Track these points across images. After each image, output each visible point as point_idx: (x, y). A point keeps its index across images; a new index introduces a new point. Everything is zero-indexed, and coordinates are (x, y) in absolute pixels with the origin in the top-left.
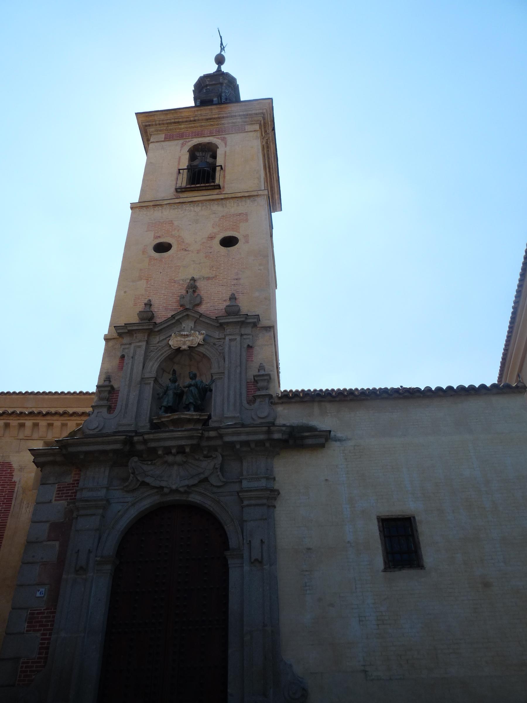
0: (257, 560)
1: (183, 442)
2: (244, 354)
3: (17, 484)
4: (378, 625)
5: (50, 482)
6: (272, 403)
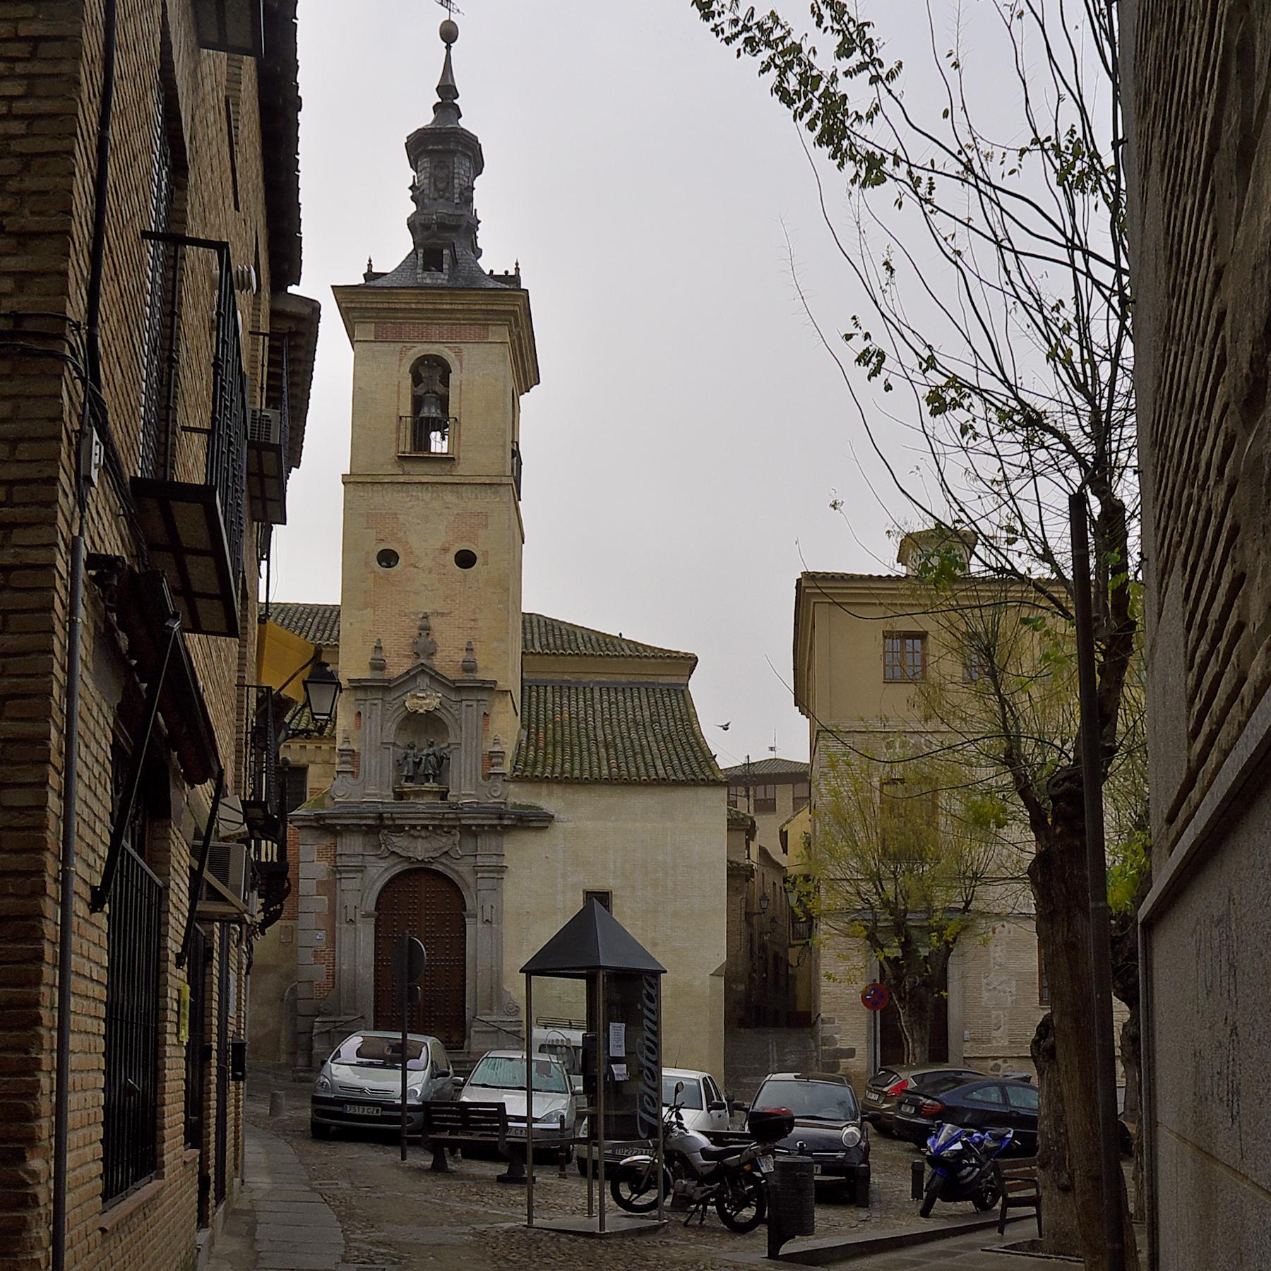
1: (426, 822)
2: (481, 723)
5: (208, 805)
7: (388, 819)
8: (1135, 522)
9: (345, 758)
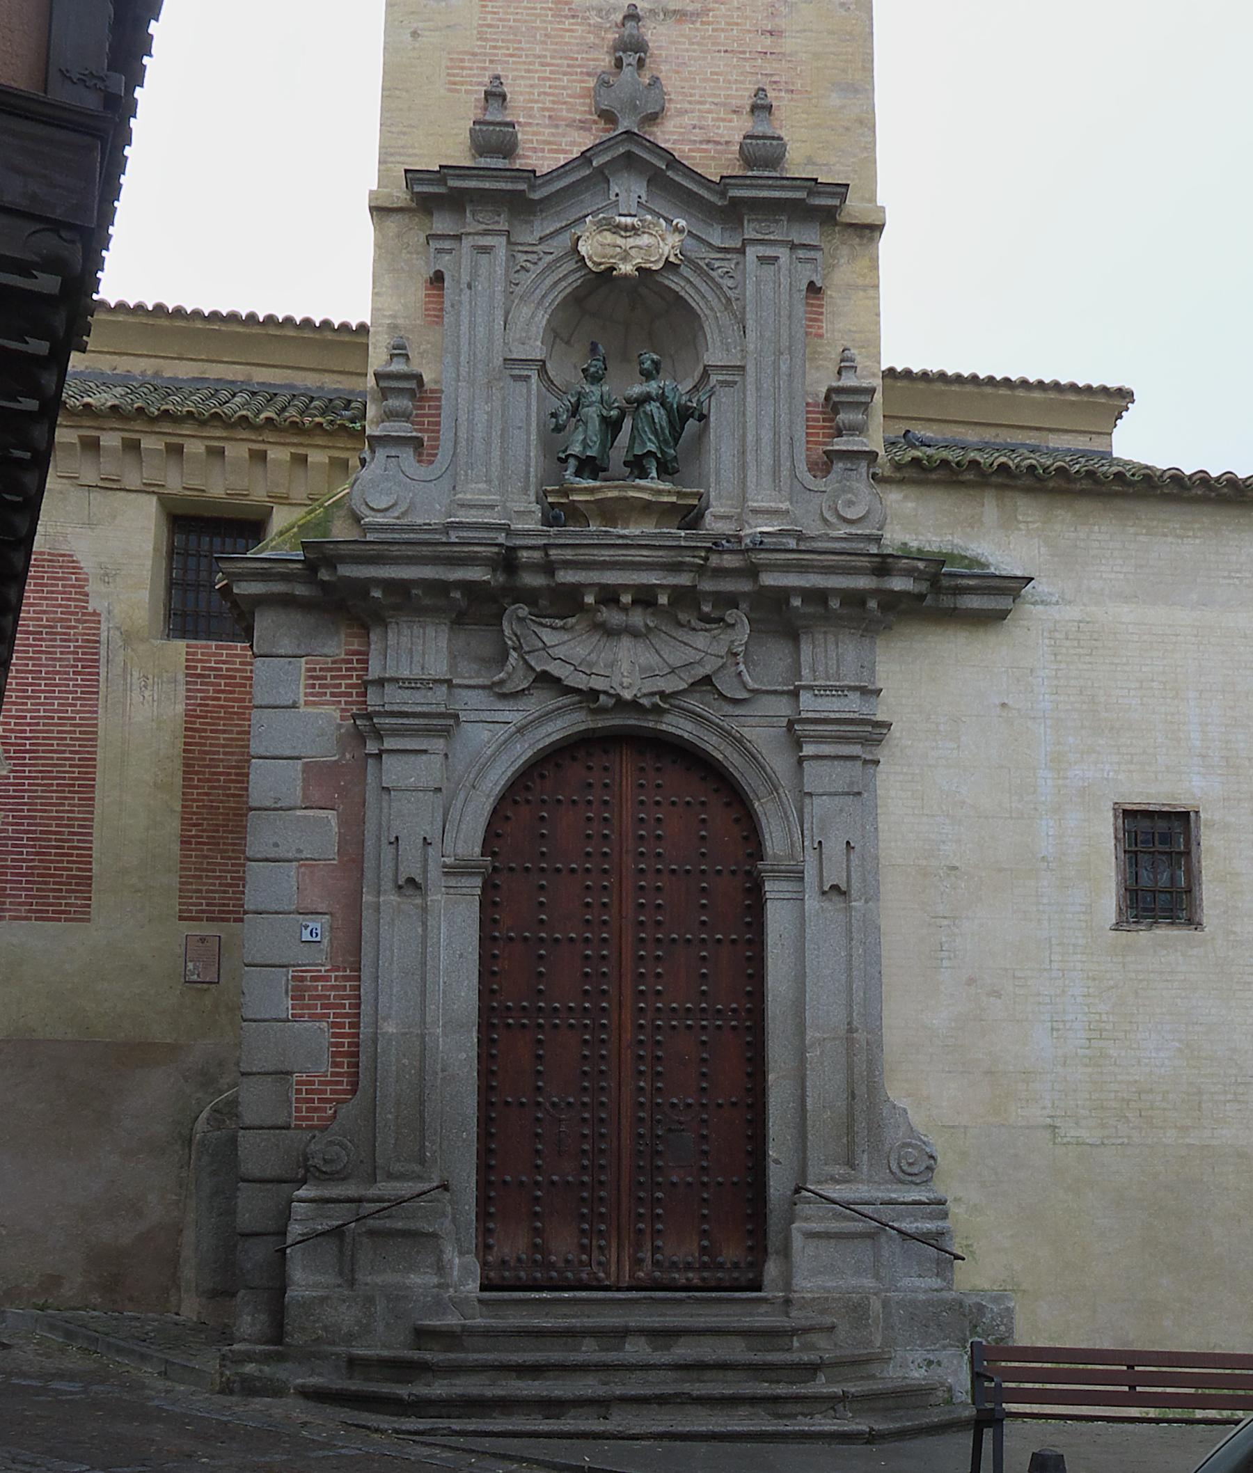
0: (835, 888)
1: (652, 579)
2: (800, 309)
3: (103, 619)
4: (1089, 1040)
5: (282, 652)
6: (874, 476)
7: (533, 567)
8: (865, 1156)
9: (394, 403)
